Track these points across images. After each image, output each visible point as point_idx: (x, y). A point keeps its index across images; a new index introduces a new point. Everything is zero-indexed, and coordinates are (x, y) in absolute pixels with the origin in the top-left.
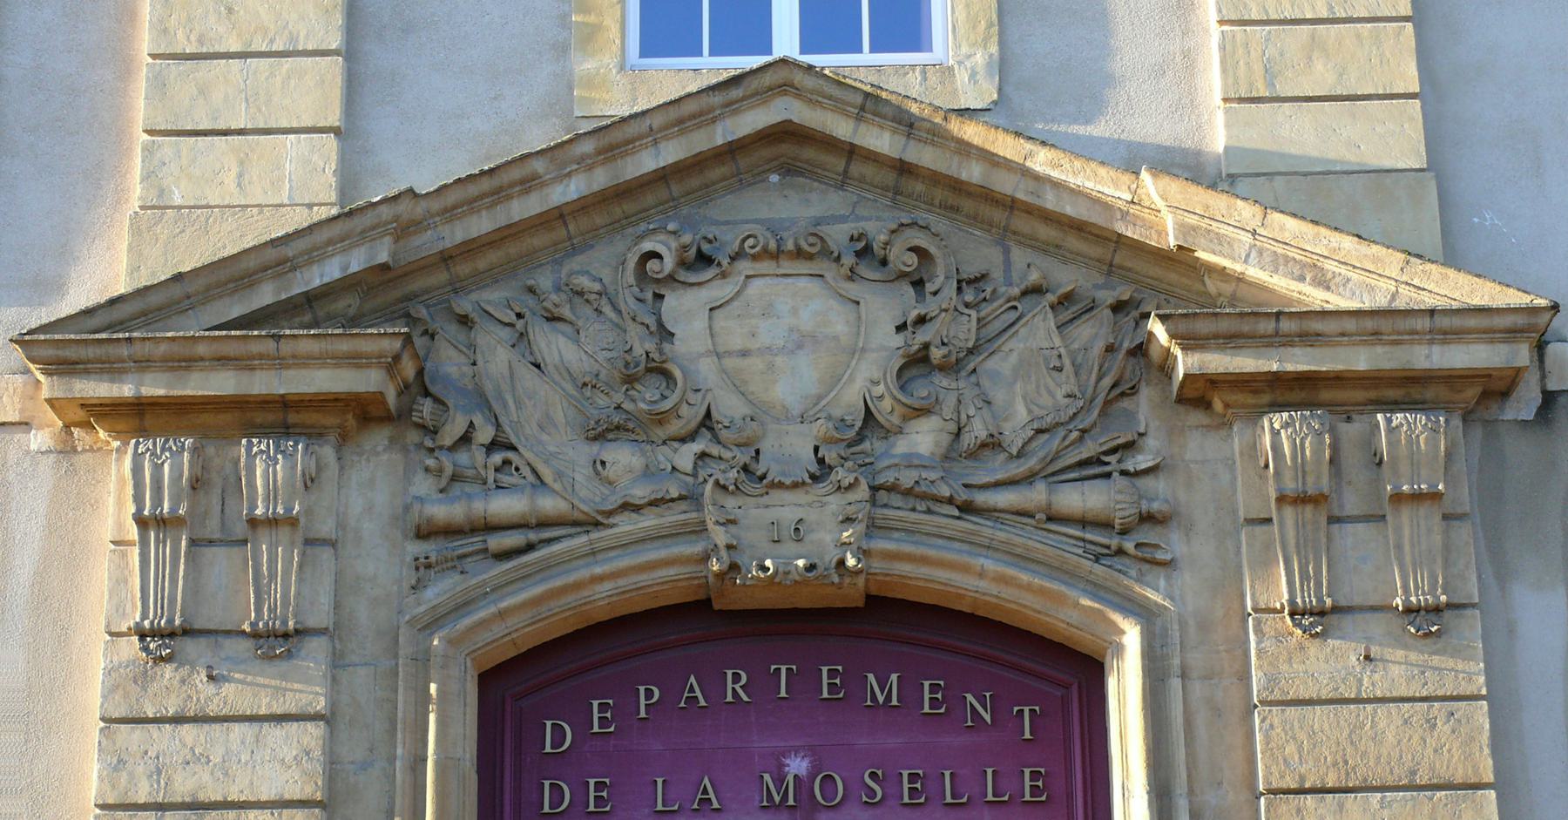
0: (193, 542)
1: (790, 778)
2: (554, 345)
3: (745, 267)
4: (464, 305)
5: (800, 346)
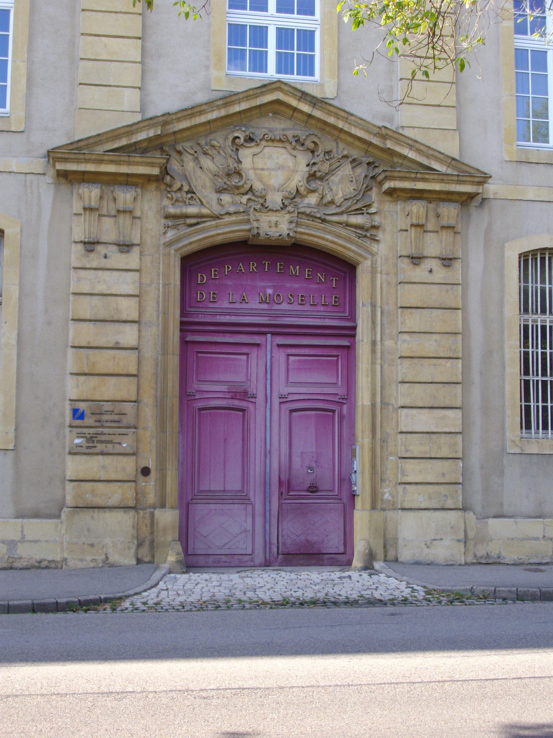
0: (100, 215)
1: (268, 295)
2: (206, 162)
3: (264, 143)
4: (179, 148)
5: (279, 169)
